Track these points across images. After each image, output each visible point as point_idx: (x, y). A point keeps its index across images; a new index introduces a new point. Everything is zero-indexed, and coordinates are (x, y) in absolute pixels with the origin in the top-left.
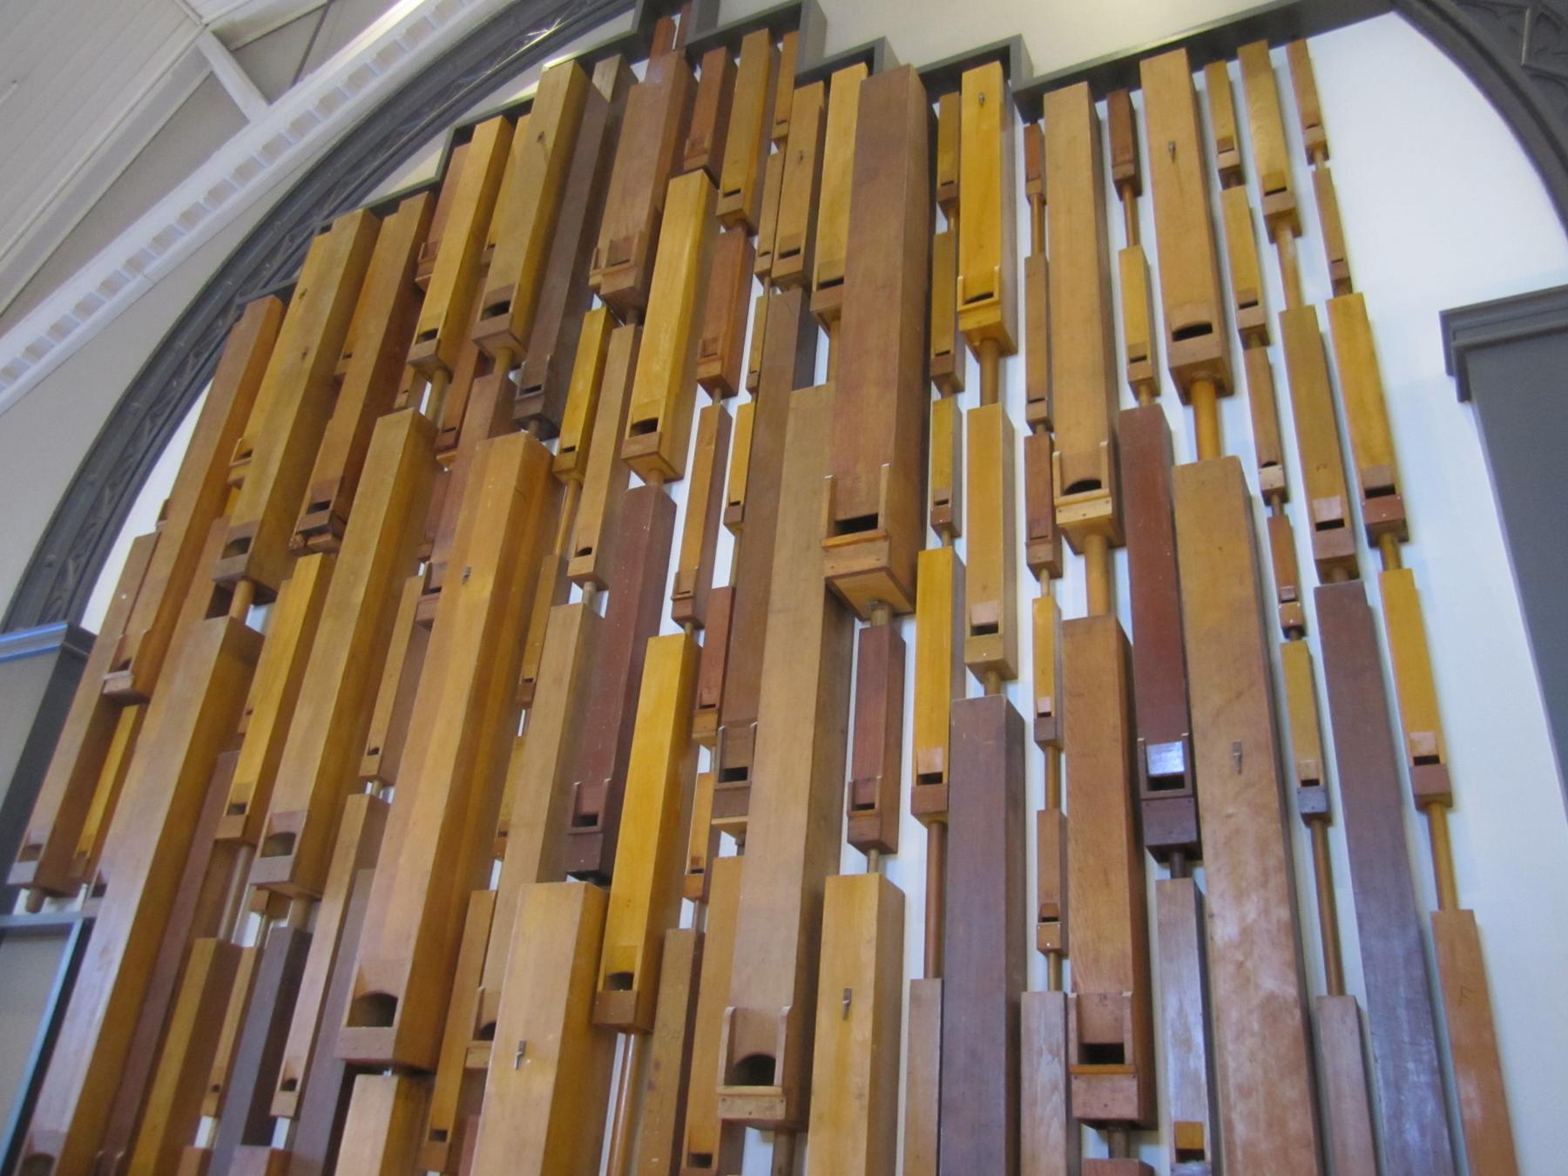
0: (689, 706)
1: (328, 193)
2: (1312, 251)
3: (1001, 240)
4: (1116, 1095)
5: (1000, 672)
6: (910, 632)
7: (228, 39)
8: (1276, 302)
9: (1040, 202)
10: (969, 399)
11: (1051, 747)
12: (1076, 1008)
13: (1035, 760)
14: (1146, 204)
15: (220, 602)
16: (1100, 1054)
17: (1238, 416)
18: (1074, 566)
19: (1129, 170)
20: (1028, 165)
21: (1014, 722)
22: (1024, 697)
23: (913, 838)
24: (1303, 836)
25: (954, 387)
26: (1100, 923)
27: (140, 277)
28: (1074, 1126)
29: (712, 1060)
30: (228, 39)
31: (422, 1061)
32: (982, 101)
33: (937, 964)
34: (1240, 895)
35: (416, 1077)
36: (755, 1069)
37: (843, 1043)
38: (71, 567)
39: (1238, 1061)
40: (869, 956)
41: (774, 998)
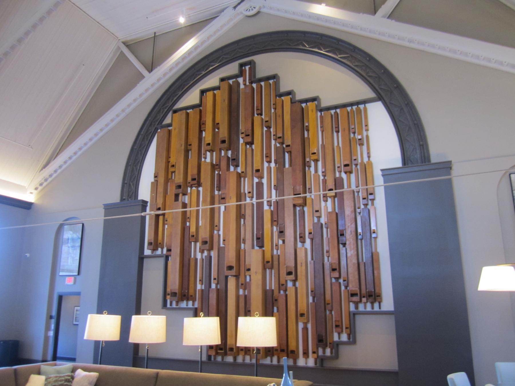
0: (272, 221)
1: (169, 99)
2: (365, 147)
3: (317, 138)
4: (336, 274)
5: (319, 217)
6: (306, 209)
7: (124, 43)
8: (360, 161)
9: (322, 132)
10: (312, 169)
11: (327, 228)
12: (331, 264)
13: (325, 230)
14: (340, 134)
15: (177, 196)
16: (334, 270)
17: (353, 176)
18: (329, 200)
19: (337, 126)
20: (321, 124)
21: (322, 224)
22: (323, 220)
23: (308, 241)
24: (335, 134)
25: (309, 167)
26: (334, 254)
27: (124, 113)
28: (331, 278)
29: (283, 272)
30: (124, 43)
31: (237, 274)
32: (312, 111)
33: (312, 259)
34: (351, 250)
35: (237, 276)
36: (289, 273)
37: (301, 270)
38: (131, 184)
39: (350, 270)
40: (304, 258)
41: (292, 264)
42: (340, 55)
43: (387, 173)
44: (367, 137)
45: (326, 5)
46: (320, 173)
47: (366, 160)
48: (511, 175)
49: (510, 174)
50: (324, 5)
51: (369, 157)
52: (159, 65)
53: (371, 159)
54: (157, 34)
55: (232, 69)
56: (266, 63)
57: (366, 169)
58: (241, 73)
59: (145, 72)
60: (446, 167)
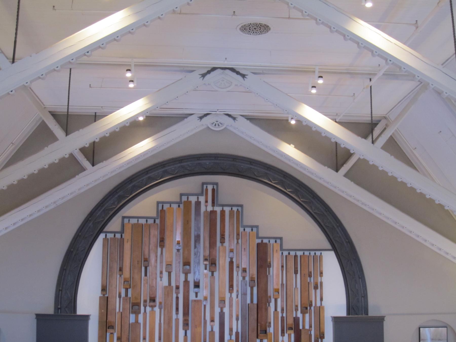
2: (318, 291)
7: (50, 112)
10: (272, 305)
42: (302, 198)
43: (337, 320)
44: (321, 283)
45: (295, 147)
46: (279, 309)
47: (318, 304)
48: (421, 329)
49: (419, 328)
50: (294, 146)
51: (321, 299)
52: (106, 159)
53: (323, 302)
54: (97, 114)
55: (191, 184)
56: (232, 187)
57: (320, 311)
58: (203, 192)
59: (86, 163)
60: (380, 320)
